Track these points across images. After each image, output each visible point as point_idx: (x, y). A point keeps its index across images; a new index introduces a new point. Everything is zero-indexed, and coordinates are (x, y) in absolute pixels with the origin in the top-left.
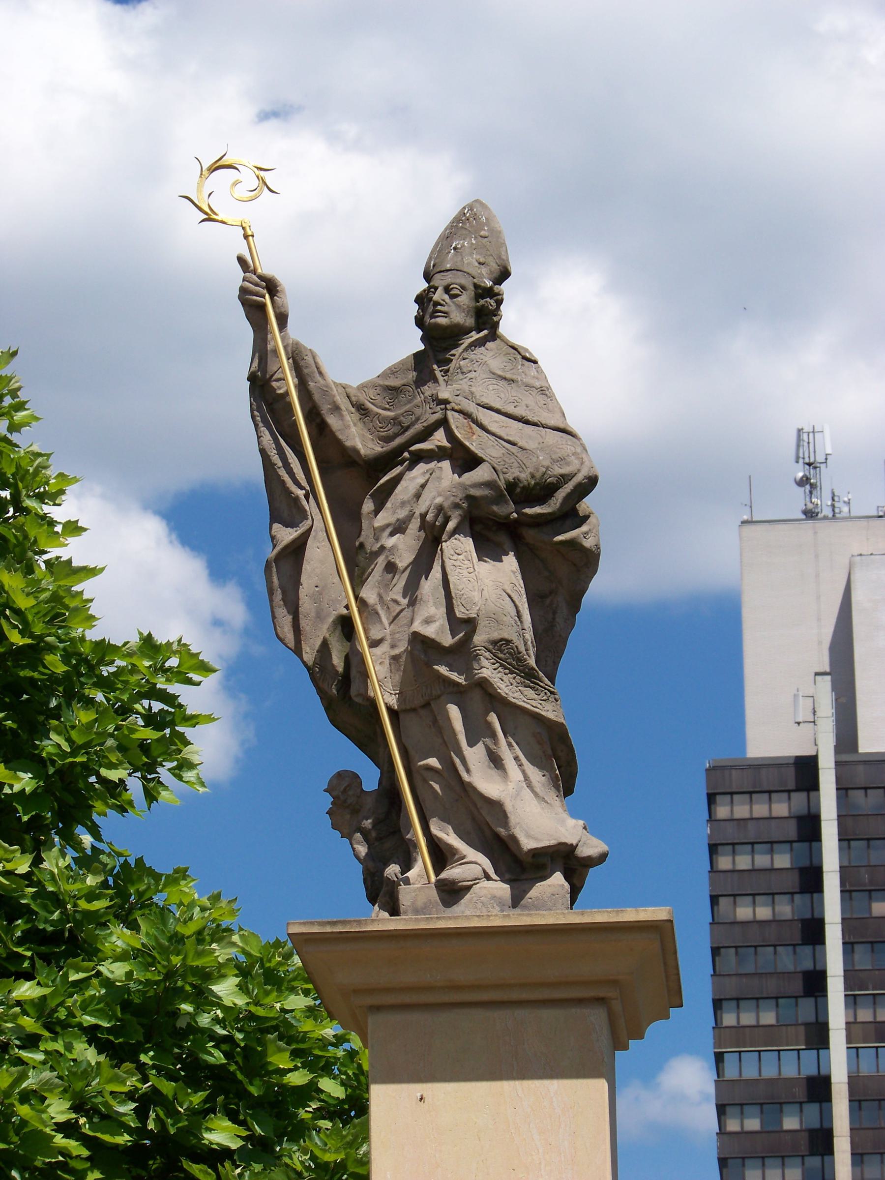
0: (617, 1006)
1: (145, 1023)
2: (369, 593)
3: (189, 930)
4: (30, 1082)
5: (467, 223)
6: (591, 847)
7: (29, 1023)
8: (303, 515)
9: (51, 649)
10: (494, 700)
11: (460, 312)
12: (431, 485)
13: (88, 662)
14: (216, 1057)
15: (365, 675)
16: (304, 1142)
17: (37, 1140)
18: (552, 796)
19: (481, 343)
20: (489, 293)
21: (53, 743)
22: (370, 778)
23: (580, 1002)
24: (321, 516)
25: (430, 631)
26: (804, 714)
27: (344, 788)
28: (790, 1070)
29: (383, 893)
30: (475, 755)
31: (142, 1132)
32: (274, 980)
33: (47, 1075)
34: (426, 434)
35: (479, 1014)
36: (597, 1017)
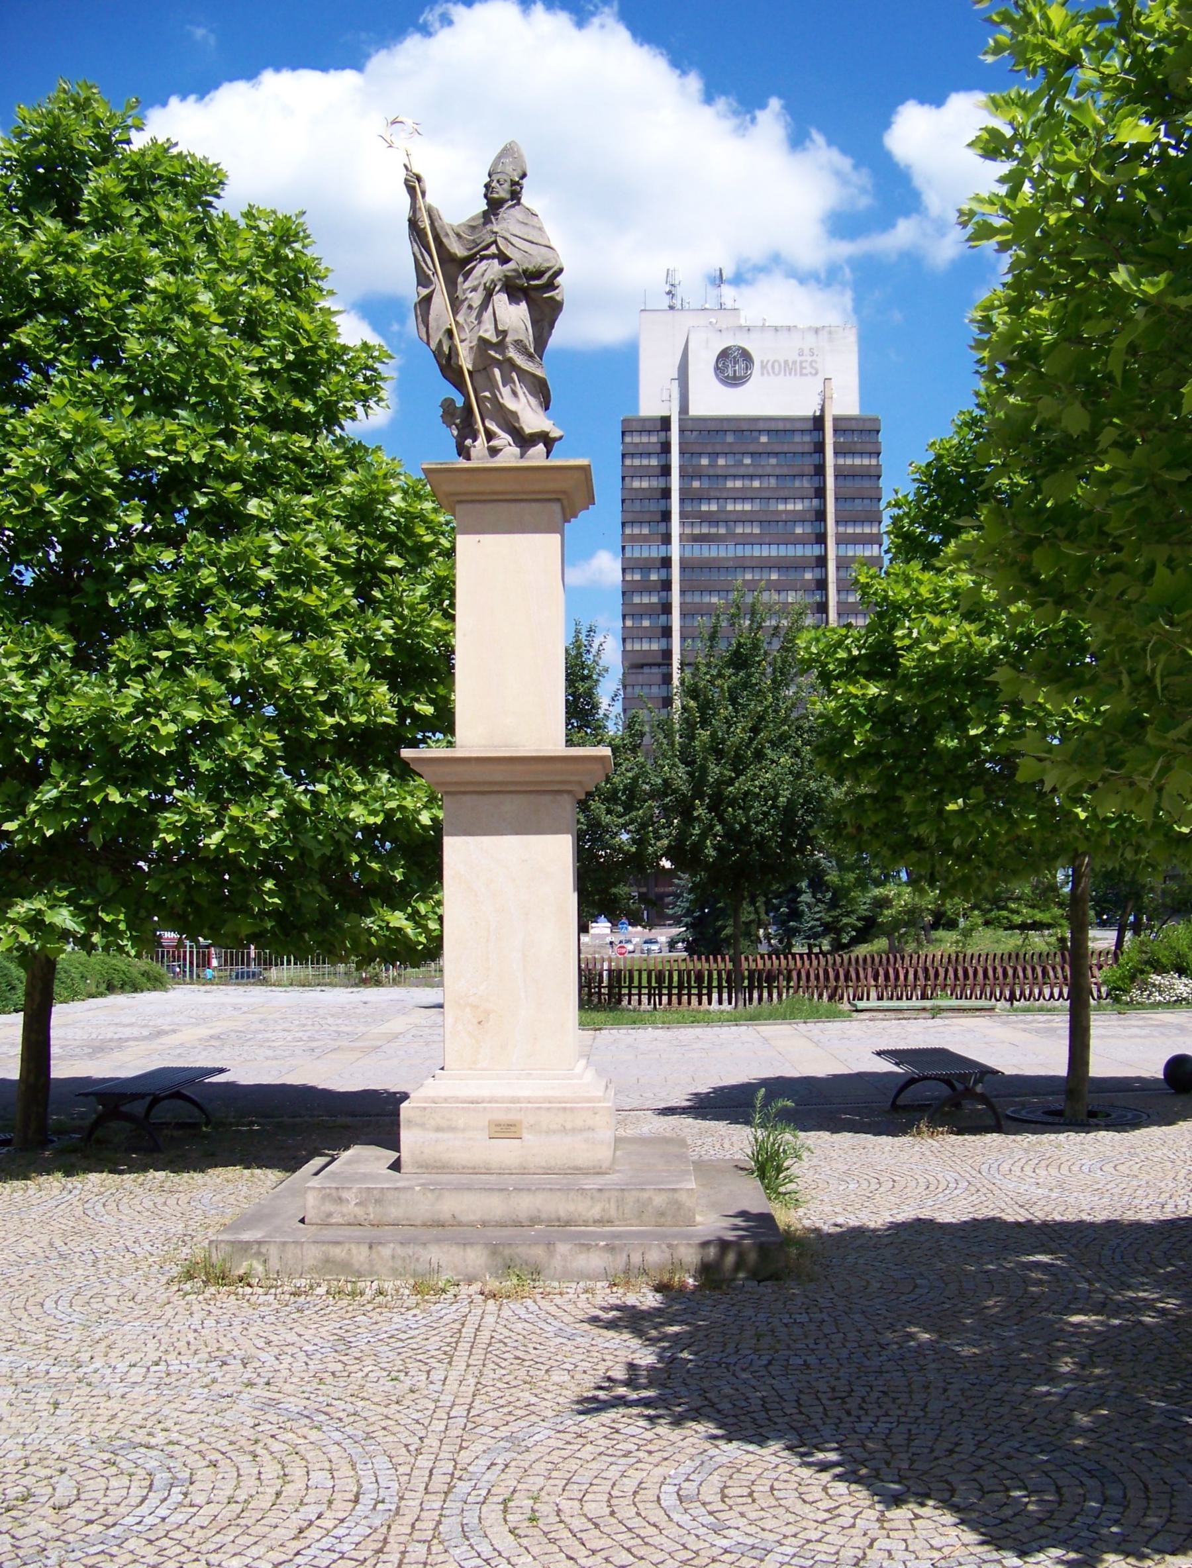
0: (565, 502)
1: (362, 514)
2: (460, 318)
3: (380, 474)
4: (309, 539)
5: (508, 151)
6: (555, 433)
7: (308, 514)
8: (431, 283)
9: (320, 348)
10: (514, 367)
11: (502, 195)
12: (488, 271)
13: (338, 353)
14: (393, 529)
15: (458, 355)
16: (342, 428)
17: (313, 564)
18: (540, 411)
19: (513, 206)
20: (517, 183)
21: (322, 390)
22: (460, 402)
23: (549, 500)
24: (439, 283)
25: (487, 336)
26: (666, 397)
27: (448, 405)
28: (654, 554)
29: (463, 452)
30: (506, 391)
31: (358, 559)
32: (418, 496)
33: (317, 535)
34: (487, 247)
35: (505, 505)
36: (556, 507)
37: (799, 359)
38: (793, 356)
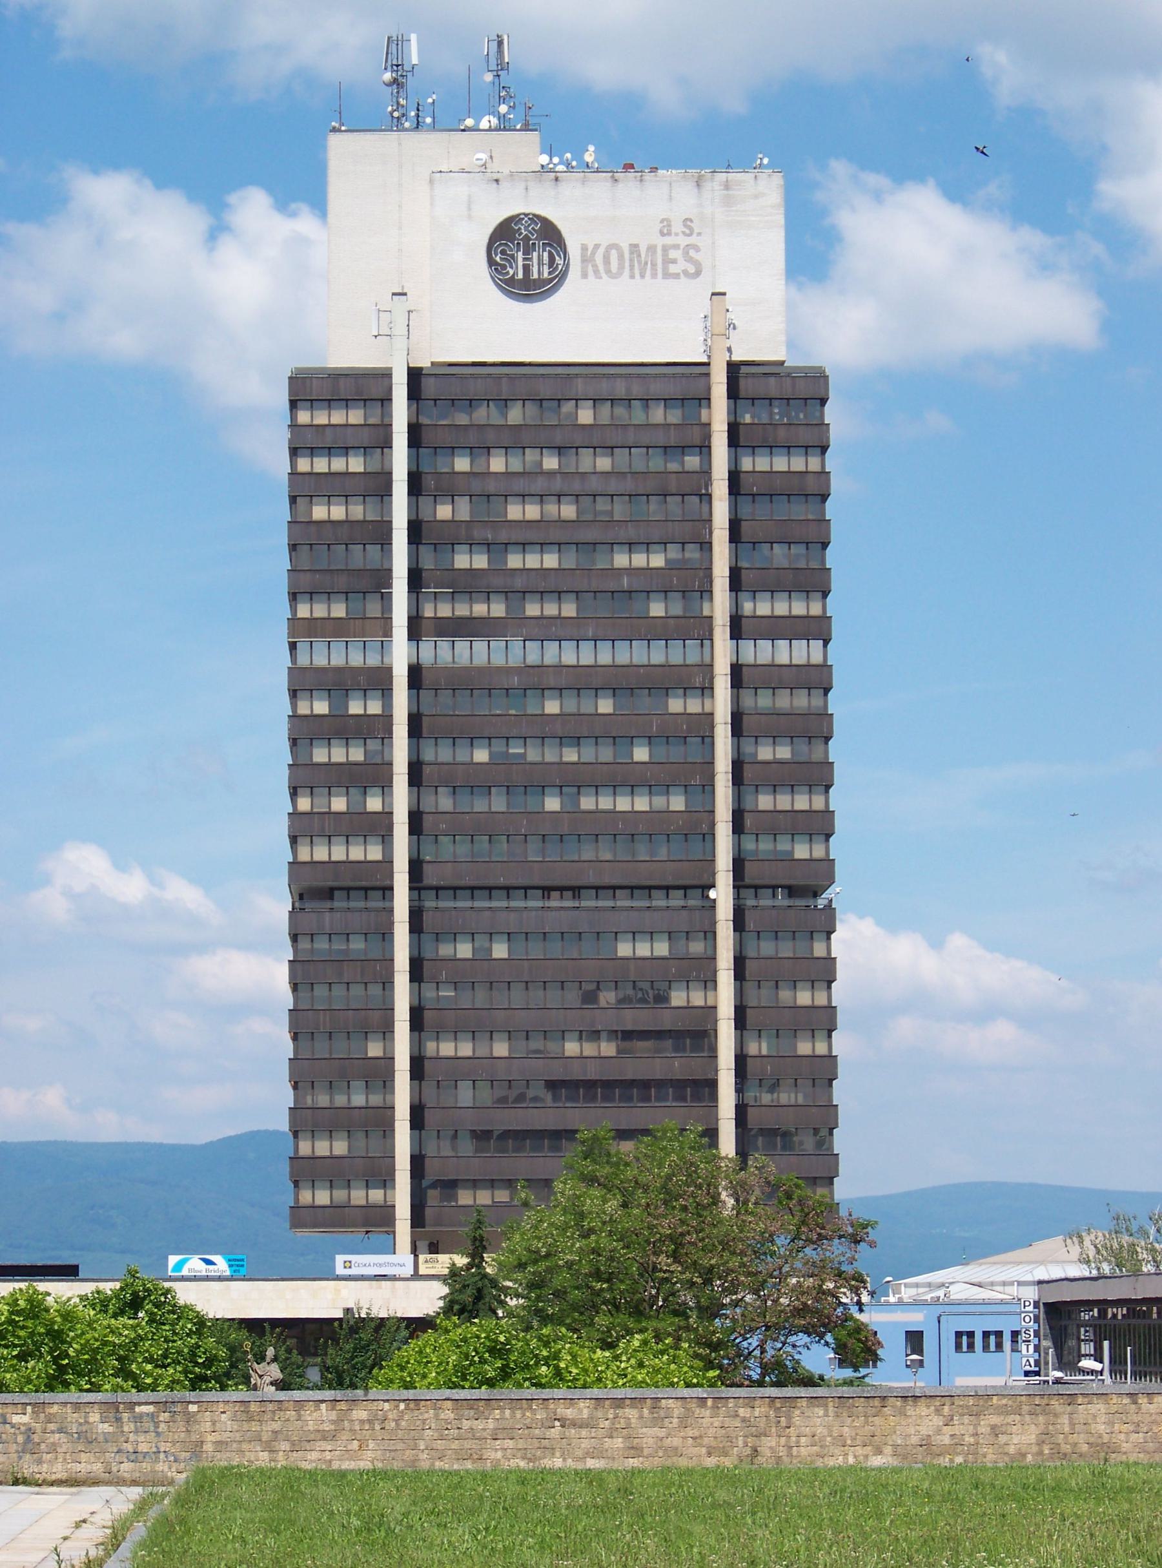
37: (660, 241)
38: (649, 237)
